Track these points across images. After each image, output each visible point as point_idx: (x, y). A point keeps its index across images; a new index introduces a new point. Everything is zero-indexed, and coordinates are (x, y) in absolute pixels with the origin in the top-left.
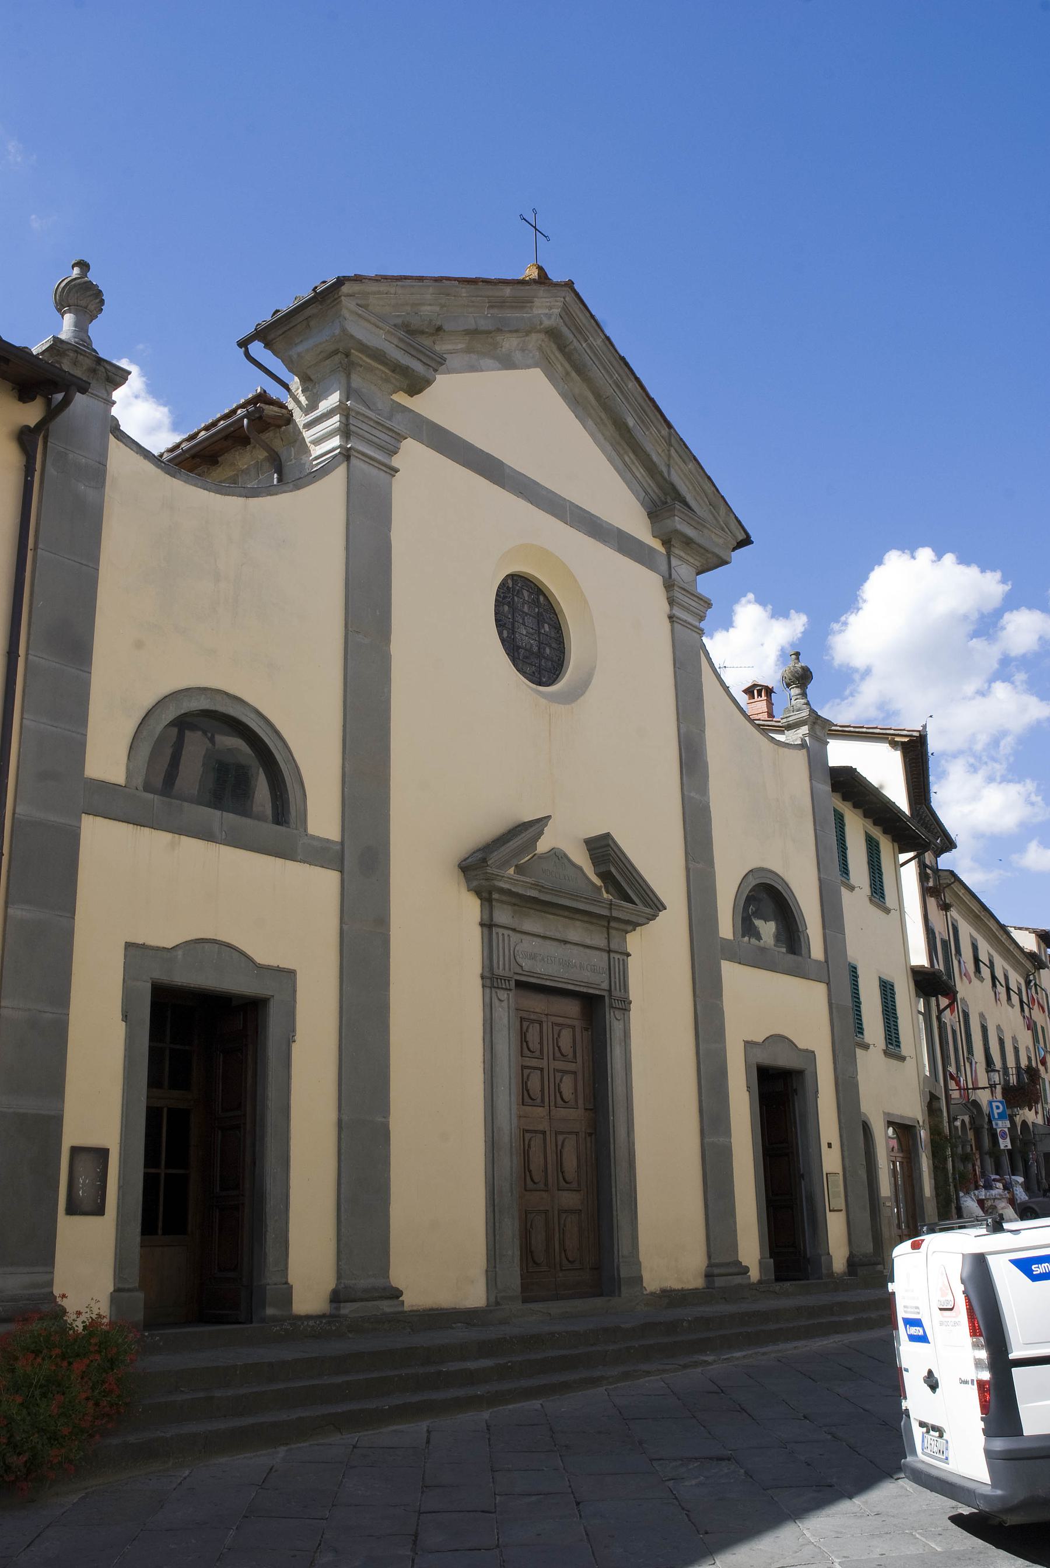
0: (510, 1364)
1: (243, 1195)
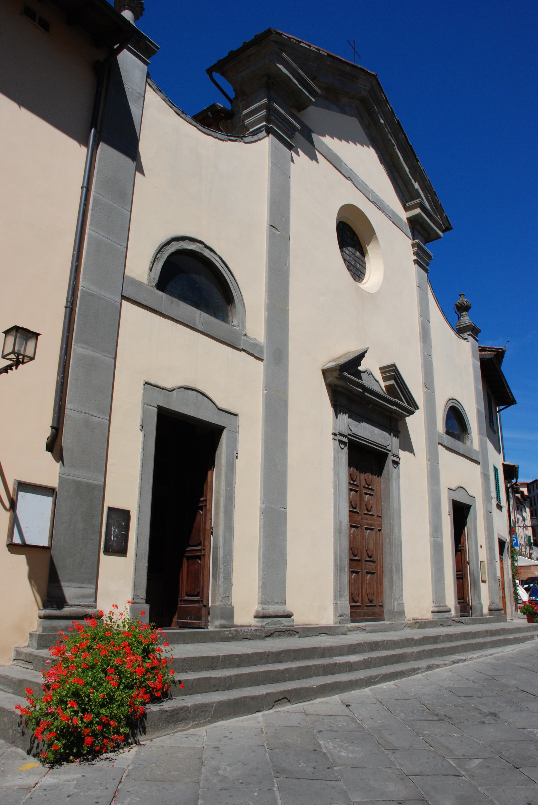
0: (369, 659)
1: (204, 550)
